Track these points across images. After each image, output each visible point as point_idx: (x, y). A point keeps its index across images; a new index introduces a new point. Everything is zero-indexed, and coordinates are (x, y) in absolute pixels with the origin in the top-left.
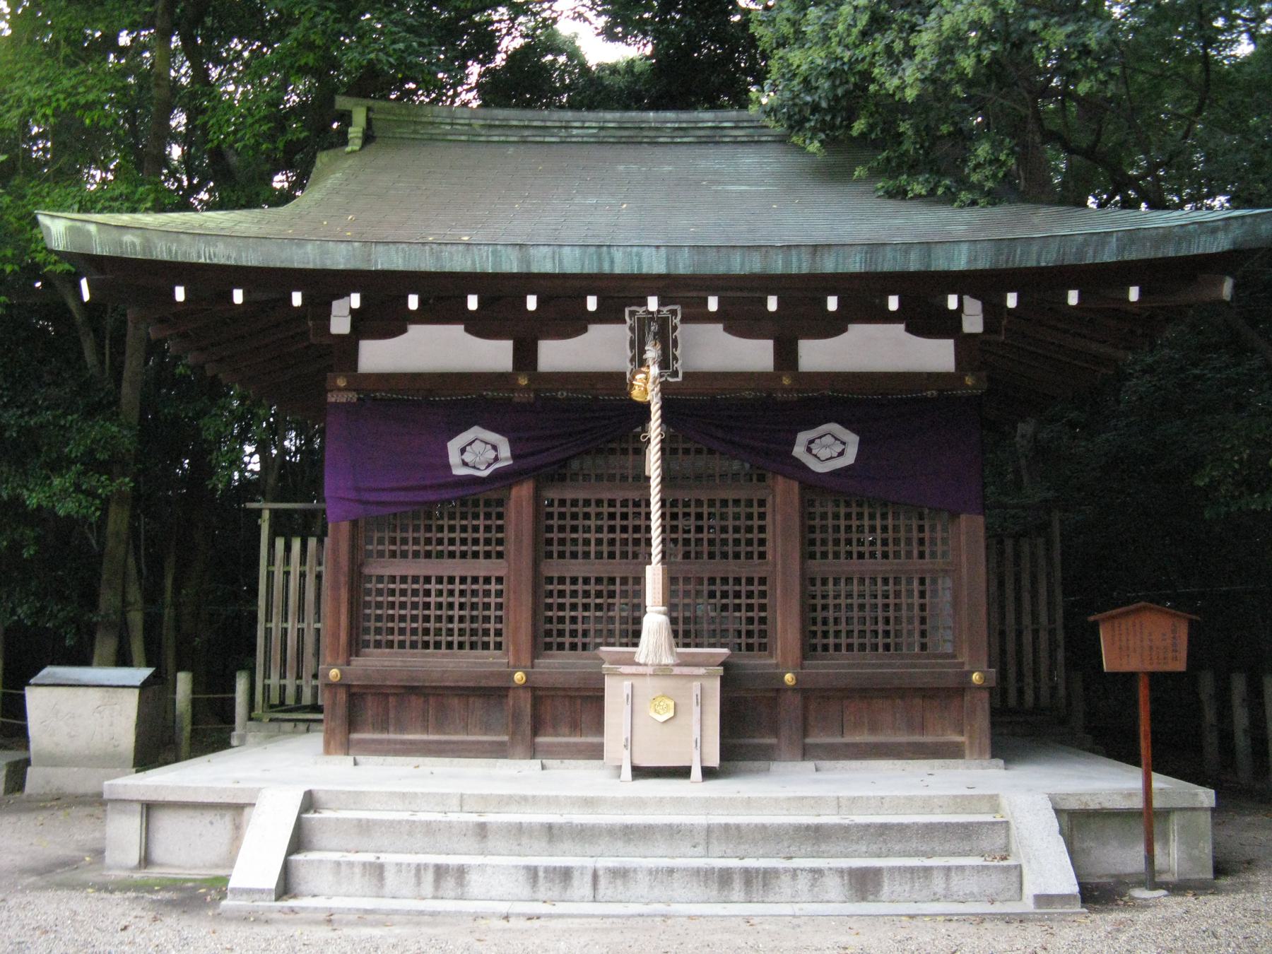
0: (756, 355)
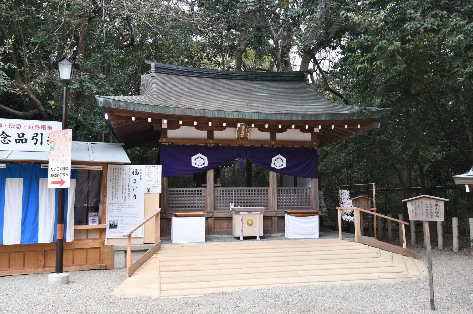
0: (266, 136)
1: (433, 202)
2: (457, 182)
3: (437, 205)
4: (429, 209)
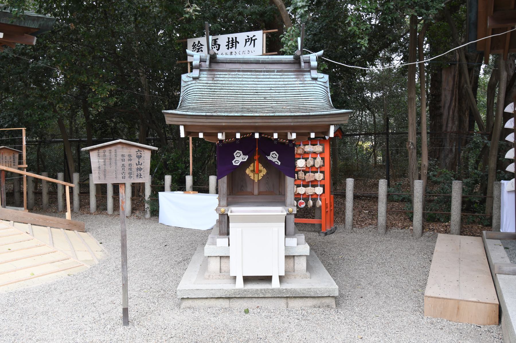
1: (133, 151)
2: (169, 121)
3: (139, 157)
4: (127, 163)
